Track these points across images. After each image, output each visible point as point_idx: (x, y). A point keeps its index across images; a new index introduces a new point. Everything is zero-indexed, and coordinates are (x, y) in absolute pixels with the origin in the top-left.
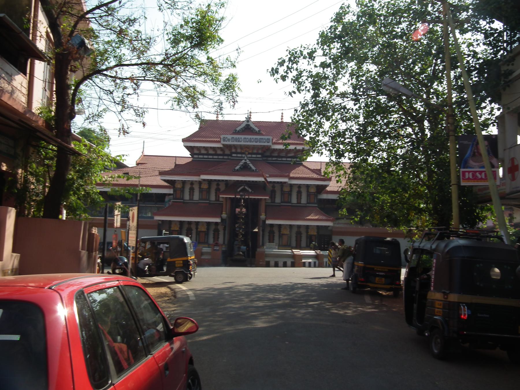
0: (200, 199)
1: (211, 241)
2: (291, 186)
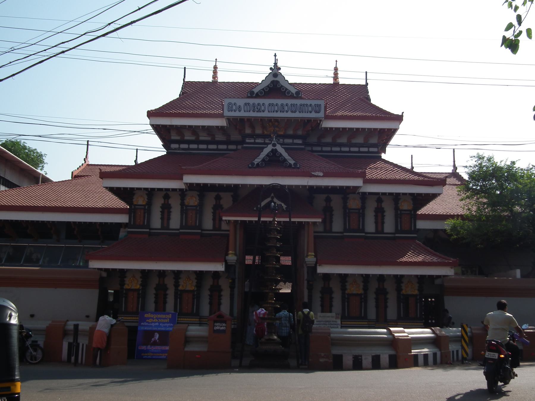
0: (182, 227)
1: (205, 310)
2: (364, 196)
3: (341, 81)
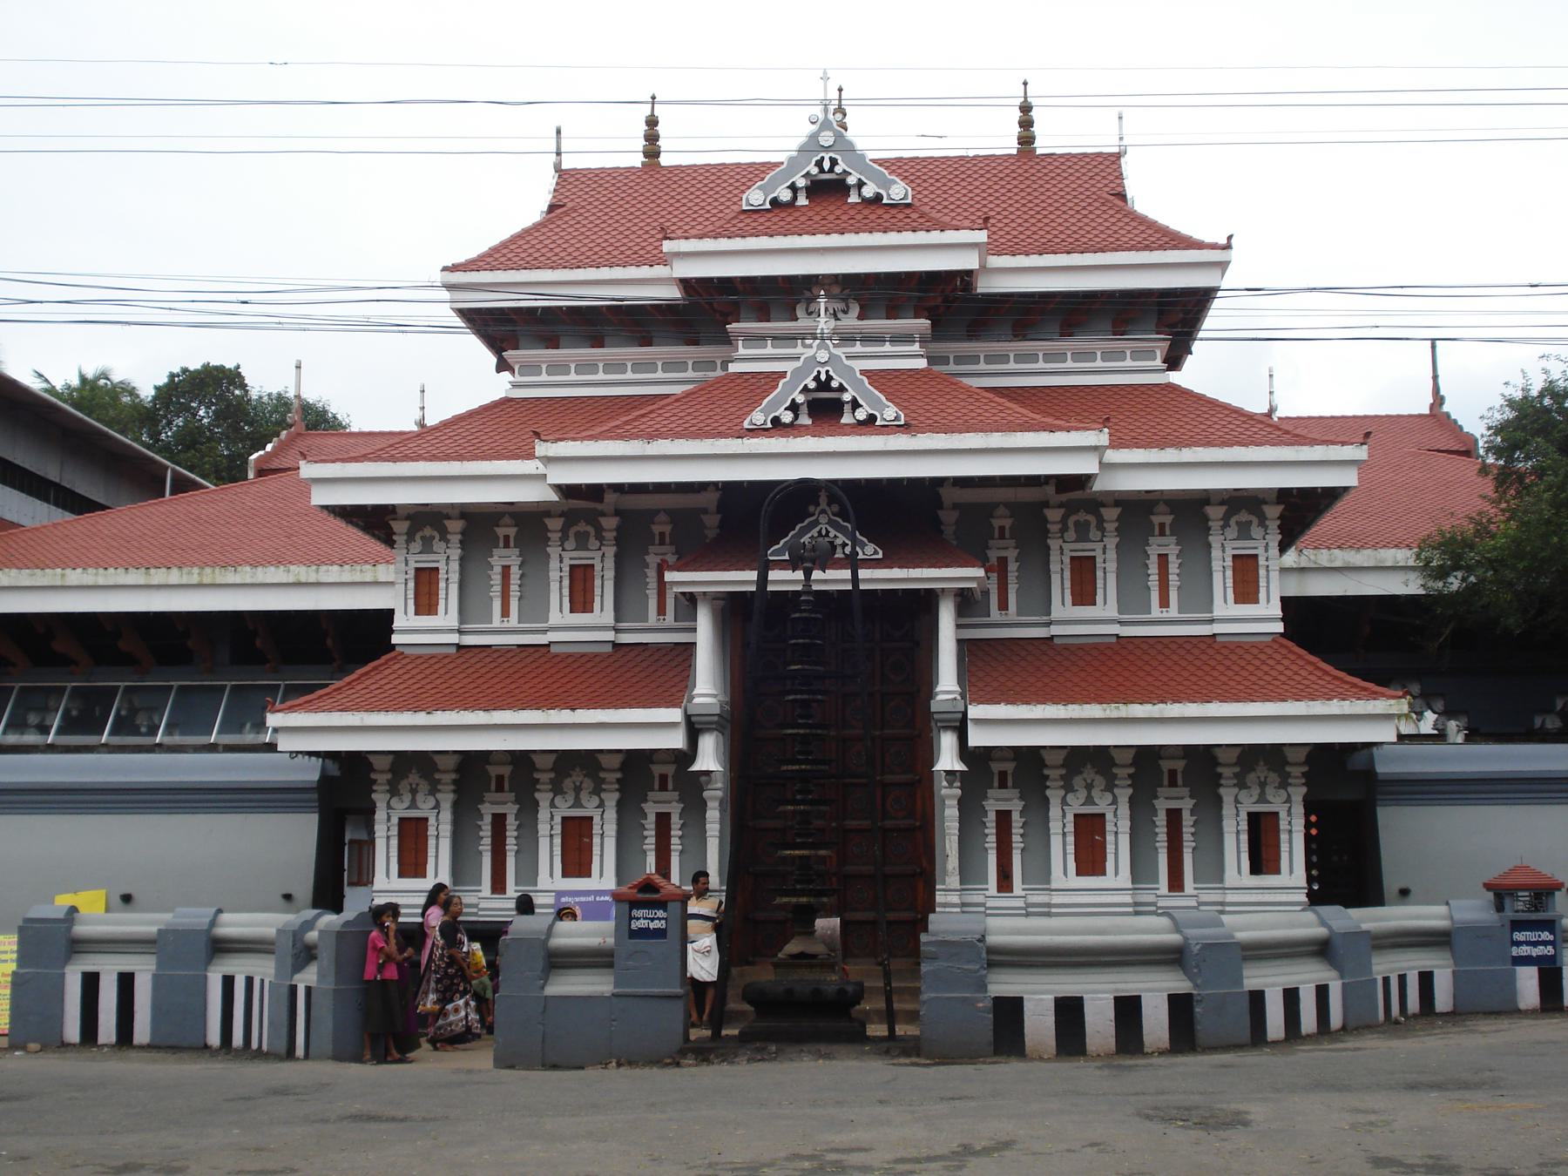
3: (1043, 145)
